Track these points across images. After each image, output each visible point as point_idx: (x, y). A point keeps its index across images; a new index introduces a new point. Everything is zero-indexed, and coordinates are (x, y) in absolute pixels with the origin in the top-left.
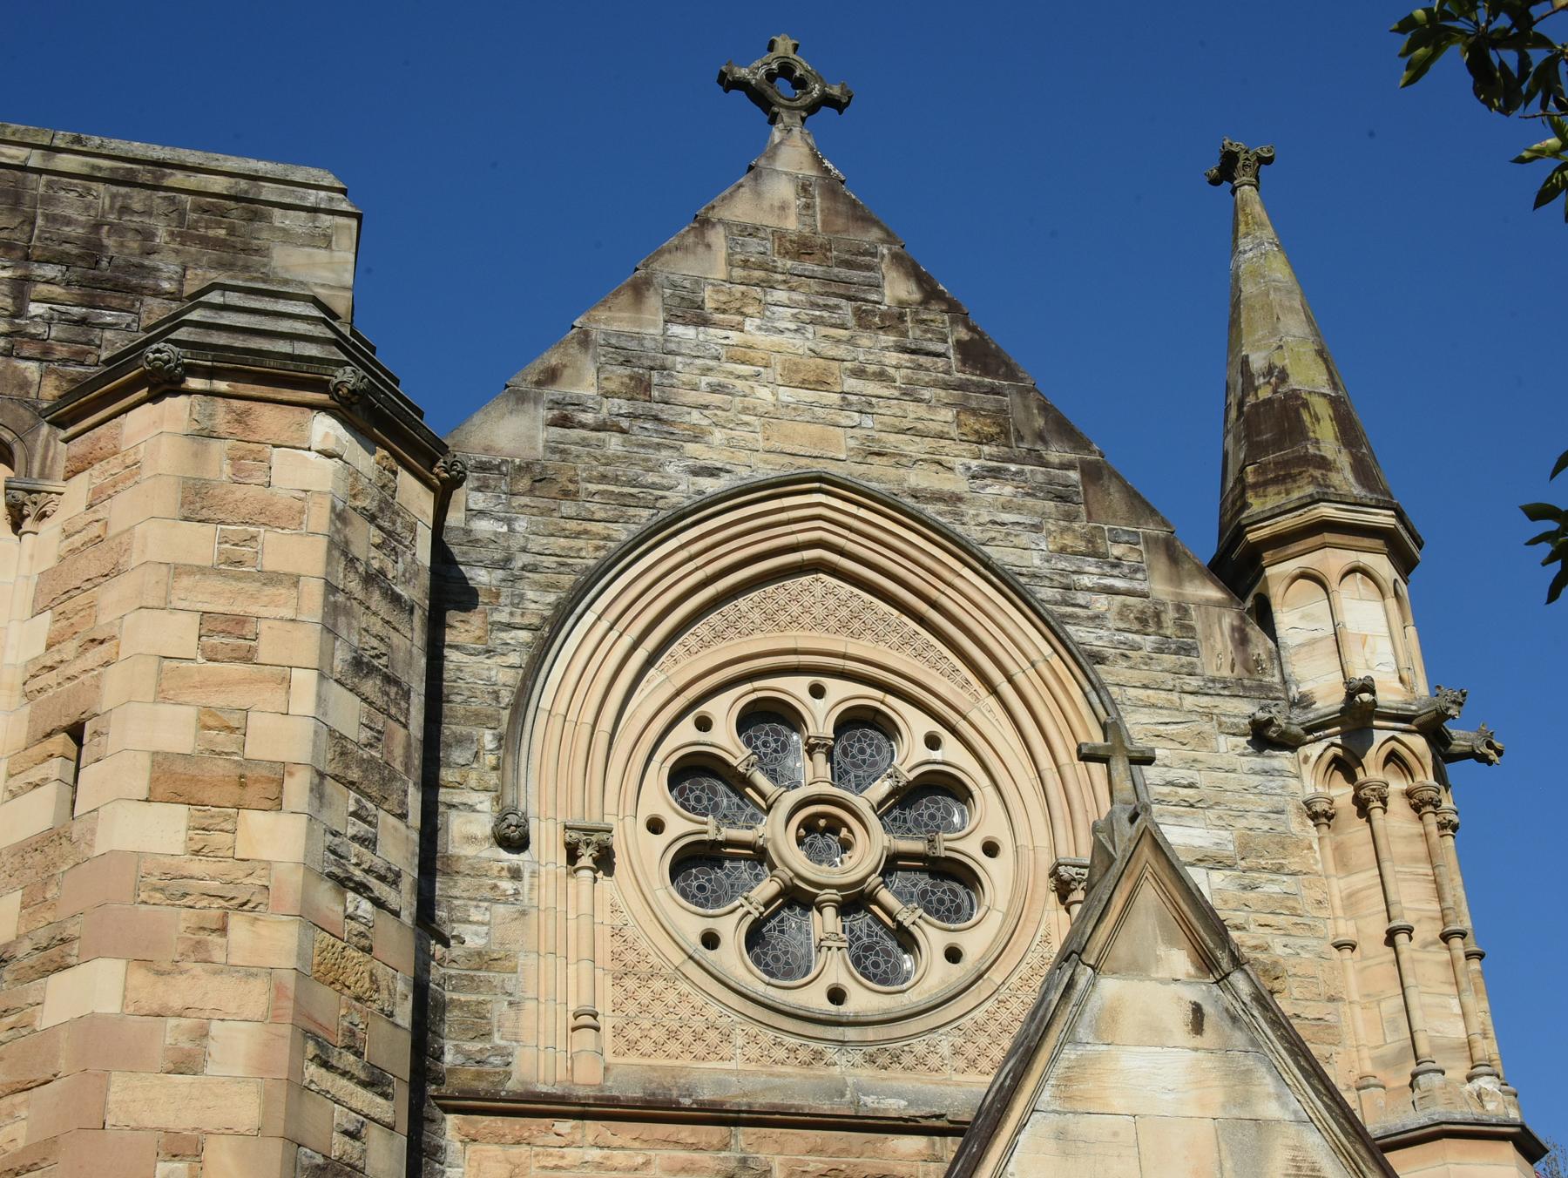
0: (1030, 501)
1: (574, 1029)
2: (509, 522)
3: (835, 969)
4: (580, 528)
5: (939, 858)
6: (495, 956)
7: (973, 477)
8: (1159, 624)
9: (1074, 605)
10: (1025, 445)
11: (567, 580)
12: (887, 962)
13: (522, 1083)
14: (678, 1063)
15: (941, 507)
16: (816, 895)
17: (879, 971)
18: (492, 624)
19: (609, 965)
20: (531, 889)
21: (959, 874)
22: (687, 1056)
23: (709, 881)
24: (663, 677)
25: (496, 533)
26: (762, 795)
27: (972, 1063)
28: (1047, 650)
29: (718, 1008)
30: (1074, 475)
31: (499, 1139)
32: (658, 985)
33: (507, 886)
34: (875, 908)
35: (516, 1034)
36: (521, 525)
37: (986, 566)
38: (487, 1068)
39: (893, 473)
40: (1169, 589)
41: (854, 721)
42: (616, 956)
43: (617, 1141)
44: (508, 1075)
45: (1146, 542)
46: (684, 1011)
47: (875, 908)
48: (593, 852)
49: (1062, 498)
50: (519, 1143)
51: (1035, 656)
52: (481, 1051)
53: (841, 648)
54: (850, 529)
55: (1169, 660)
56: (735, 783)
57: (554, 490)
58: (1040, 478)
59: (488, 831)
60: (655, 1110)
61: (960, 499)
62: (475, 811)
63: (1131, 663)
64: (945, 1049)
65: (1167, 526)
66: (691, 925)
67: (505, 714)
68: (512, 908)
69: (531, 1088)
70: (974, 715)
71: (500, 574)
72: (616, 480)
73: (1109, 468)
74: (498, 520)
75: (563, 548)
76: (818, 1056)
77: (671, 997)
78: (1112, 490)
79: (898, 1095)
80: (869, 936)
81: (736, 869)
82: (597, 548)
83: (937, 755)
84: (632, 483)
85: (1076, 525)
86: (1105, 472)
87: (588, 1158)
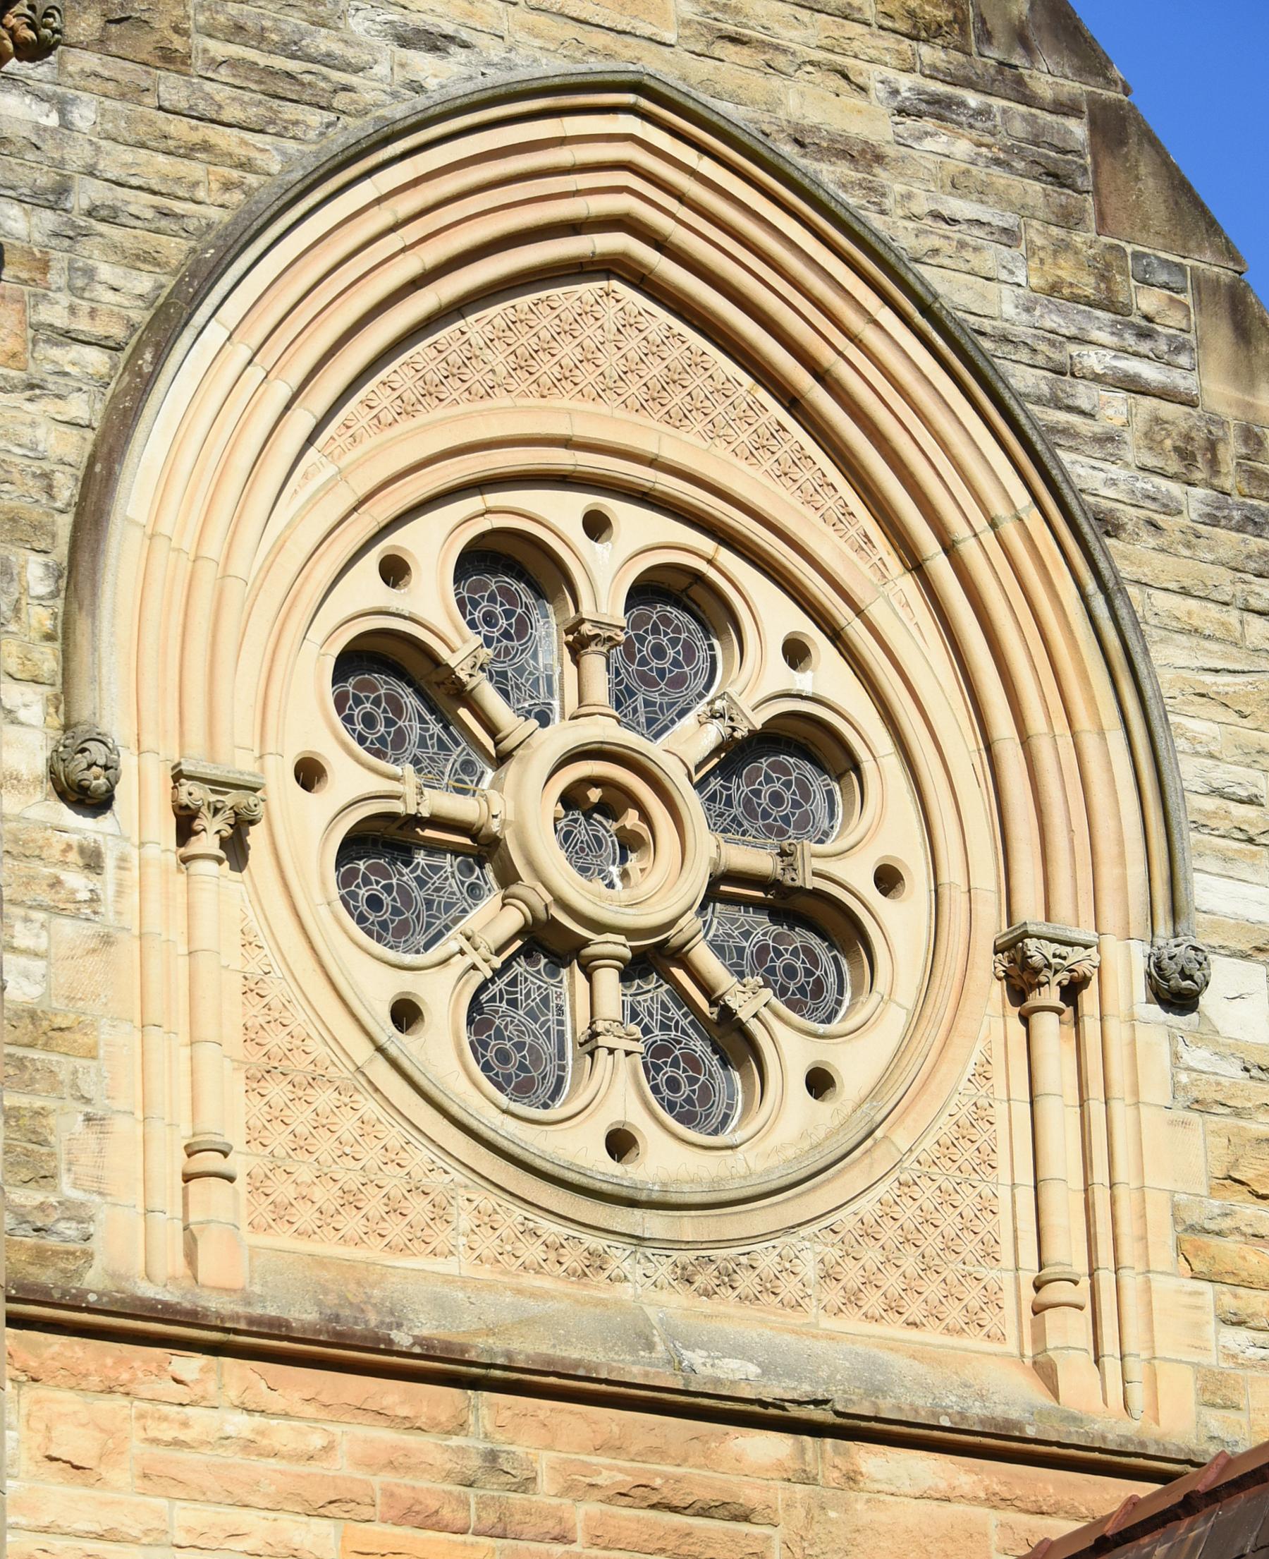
0: (1000, 177)
1: (188, 1178)
2: (62, 105)
3: (618, 1089)
4: (196, 137)
5: (801, 890)
6: (59, 1022)
7: (901, 111)
8: (1214, 464)
9: (1070, 409)
10: (995, 53)
11: (174, 249)
12: (692, 1081)
13: (113, 1276)
14: (359, 1254)
15: (843, 170)
16: (586, 943)
17: (679, 1098)
18: (37, 327)
19: (240, 1053)
20: (120, 893)
21: (837, 925)
22: (374, 1240)
23: (388, 889)
24: (331, 470)
25: (39, 129)
26: (492, 729)
27: (853, 1299)
28: (1022, 498)
29: (427, 1158)
30: (1078, 130)
31: (76, 1380)
32: (324, 1098)
33: (77, 881)
34: (679, 974)
35: (99, 1179)
36: (84, 115)
37: (926, 310)
38: (51, 1242)
39: (758, 84)
40: (1232, 393)
41: (658, 589)
42: (251, 1036)
43: (276, 1402)
44: (89, 1256)
45: (1198, 289)
46: (371, 1155)
47: (679, 974)
48: (217, 822)
49: (1057, 178)
50: (111, 1391)
51: (999, 508)
52: (42, 1207)
53: (648, 445)
54: (681, 198)
55: (1228, 542)
56: (439, 696)
57: (146, 46)
58: (1019, 128)
59: (41, 768)
60: (344, 1350)
61: (879, 158)
62: (15, 722)
63: (1162, 541)
64: (809, 1269)
65: (1235, 258)
66: (375, 981)
67: (64, 524)
68: (88, 929)
69: (126, 1285)
70: (877, 612)
71: (48, 219)
72: (260, 39)
73: (1139, 121)
74: (41, 98)
75: (165, 178)
76: (596, 1261)
77: (347, 1125)
78: (1143, 170)
79: (741, 1351)
80: (664, 1027)
81: (436, 869)
82: (227, 186)
83: (803, 681)
84: (291, 49)
85: (1078, 239)
86: (1132, 129)
87: (230, 1430)
